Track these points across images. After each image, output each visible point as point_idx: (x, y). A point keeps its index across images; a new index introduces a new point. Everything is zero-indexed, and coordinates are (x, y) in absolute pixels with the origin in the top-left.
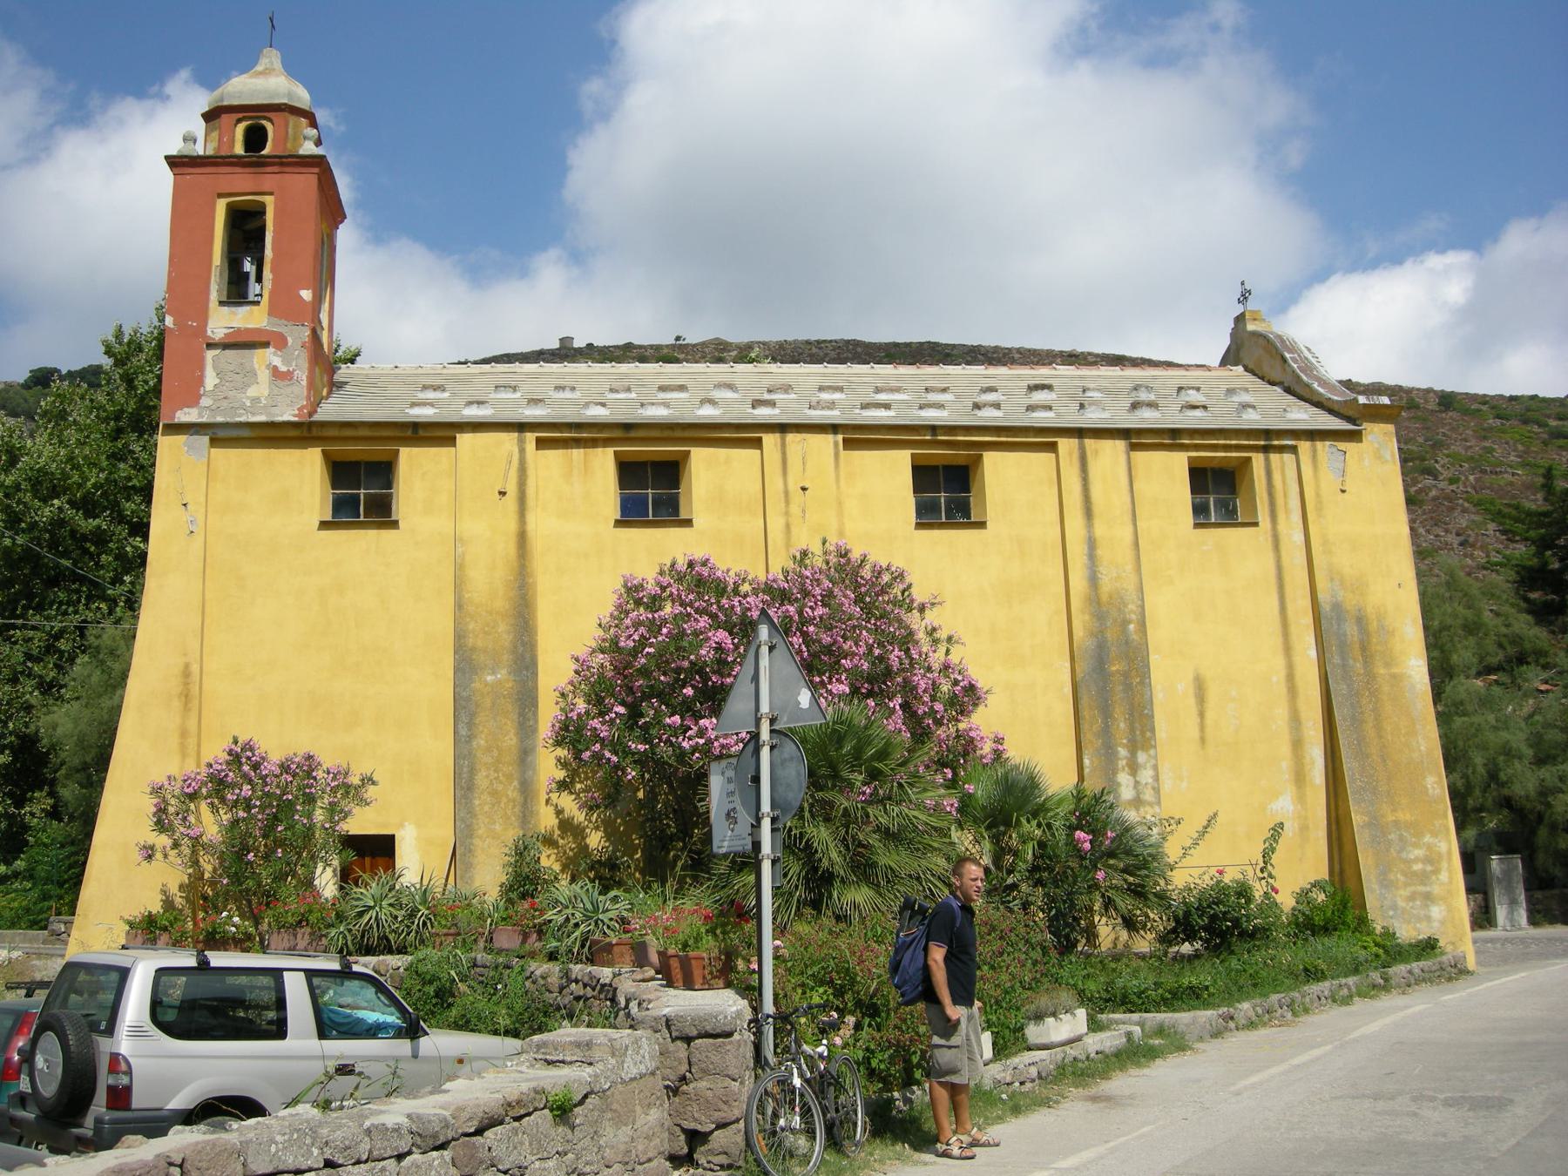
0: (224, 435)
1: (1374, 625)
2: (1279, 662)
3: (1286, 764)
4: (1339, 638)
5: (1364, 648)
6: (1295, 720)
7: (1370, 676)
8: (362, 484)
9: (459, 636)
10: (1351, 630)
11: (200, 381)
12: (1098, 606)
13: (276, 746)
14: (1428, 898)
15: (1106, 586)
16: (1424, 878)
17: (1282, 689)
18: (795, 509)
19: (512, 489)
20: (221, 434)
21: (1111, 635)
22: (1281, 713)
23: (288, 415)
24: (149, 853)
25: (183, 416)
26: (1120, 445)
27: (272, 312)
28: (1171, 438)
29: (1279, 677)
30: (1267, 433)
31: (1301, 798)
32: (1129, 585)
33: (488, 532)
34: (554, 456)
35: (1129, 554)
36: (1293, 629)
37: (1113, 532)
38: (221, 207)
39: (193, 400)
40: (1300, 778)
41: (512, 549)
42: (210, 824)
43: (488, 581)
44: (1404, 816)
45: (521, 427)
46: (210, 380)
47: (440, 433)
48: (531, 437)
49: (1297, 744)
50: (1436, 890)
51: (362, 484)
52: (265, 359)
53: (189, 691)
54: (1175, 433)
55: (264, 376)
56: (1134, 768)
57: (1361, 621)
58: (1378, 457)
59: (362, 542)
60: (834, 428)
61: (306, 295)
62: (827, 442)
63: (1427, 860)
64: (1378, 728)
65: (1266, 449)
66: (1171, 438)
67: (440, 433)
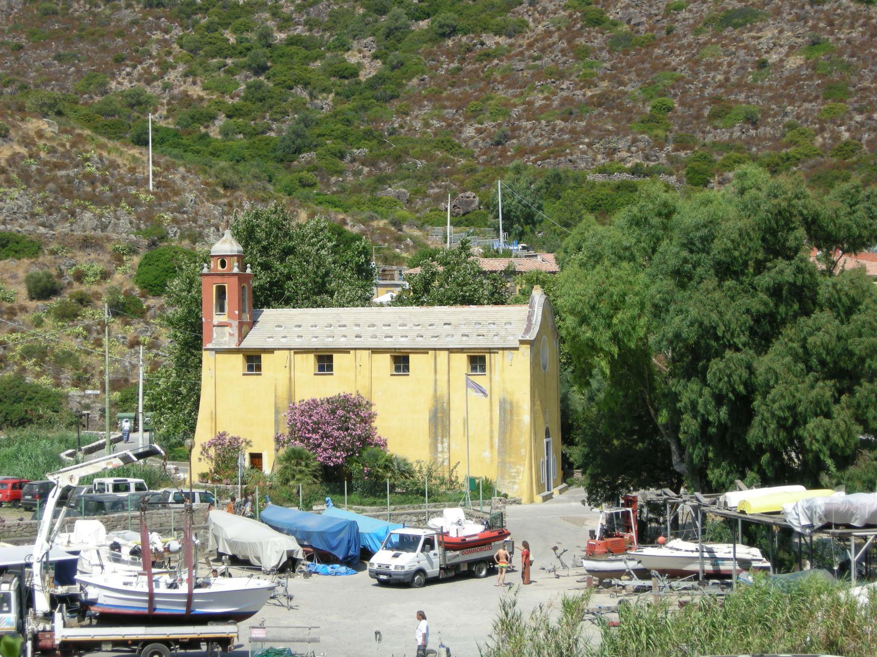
0: (218, 351)
1: (515, 405)
2: (489, 414)
3: (488, 443)
4: (507, 410)
5: (511, 411)
6: (491, 431)
7: (512, 419)
8: (253, 361)
9: (276, 404)
10: (508, 406)
11: (212, 336)
12: (436, 398)
13: (232, 433)
14: (514, 483)
15: (439, 393)
16: (514, 477)
17: (488, 422)
18: (358, 371)
19: (288, 366)
20: (25, 601)
21: (439, 406)
22: (488, 429)
23: (233, 346)
24: (200, 459)
25: (209, 346)
26: (447, 352)
27: (229, 317)
28: (461, 350)
29: (488, 418)
30: (490, 349)
31: (492, 453)
32: (446, 392)
33: (282, 377)
34: (298, 356)
35: (446, 384)
36: (493, 405)
37: (442, 377)
38: (214, 286)
39: (210, 342)
40: (492, 447)
41: (288, 381)
42: (212, 452)
43: (283, 391)
44: (512, 460)
45: (290, 349)
46: (215, 336)
47: (271, 351)
48: (292, 352)
49: (491, 438)
50: (517, 481)
51: (253, 361)
52: (227, 330)
53: (214, 418)
54: (462, 349)
55: (227, 334)
56: (442, 443)
57: (511, 404)
58: (523, 354)
59: (253, 379)
60: (369, 349)
61: (237, 312)
62: (367, 352)
63: (517, 473)
64: (511, 435)
65: (490, 353)
66: (461, 350)
67: (271, 351)
